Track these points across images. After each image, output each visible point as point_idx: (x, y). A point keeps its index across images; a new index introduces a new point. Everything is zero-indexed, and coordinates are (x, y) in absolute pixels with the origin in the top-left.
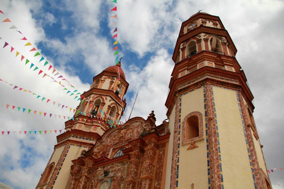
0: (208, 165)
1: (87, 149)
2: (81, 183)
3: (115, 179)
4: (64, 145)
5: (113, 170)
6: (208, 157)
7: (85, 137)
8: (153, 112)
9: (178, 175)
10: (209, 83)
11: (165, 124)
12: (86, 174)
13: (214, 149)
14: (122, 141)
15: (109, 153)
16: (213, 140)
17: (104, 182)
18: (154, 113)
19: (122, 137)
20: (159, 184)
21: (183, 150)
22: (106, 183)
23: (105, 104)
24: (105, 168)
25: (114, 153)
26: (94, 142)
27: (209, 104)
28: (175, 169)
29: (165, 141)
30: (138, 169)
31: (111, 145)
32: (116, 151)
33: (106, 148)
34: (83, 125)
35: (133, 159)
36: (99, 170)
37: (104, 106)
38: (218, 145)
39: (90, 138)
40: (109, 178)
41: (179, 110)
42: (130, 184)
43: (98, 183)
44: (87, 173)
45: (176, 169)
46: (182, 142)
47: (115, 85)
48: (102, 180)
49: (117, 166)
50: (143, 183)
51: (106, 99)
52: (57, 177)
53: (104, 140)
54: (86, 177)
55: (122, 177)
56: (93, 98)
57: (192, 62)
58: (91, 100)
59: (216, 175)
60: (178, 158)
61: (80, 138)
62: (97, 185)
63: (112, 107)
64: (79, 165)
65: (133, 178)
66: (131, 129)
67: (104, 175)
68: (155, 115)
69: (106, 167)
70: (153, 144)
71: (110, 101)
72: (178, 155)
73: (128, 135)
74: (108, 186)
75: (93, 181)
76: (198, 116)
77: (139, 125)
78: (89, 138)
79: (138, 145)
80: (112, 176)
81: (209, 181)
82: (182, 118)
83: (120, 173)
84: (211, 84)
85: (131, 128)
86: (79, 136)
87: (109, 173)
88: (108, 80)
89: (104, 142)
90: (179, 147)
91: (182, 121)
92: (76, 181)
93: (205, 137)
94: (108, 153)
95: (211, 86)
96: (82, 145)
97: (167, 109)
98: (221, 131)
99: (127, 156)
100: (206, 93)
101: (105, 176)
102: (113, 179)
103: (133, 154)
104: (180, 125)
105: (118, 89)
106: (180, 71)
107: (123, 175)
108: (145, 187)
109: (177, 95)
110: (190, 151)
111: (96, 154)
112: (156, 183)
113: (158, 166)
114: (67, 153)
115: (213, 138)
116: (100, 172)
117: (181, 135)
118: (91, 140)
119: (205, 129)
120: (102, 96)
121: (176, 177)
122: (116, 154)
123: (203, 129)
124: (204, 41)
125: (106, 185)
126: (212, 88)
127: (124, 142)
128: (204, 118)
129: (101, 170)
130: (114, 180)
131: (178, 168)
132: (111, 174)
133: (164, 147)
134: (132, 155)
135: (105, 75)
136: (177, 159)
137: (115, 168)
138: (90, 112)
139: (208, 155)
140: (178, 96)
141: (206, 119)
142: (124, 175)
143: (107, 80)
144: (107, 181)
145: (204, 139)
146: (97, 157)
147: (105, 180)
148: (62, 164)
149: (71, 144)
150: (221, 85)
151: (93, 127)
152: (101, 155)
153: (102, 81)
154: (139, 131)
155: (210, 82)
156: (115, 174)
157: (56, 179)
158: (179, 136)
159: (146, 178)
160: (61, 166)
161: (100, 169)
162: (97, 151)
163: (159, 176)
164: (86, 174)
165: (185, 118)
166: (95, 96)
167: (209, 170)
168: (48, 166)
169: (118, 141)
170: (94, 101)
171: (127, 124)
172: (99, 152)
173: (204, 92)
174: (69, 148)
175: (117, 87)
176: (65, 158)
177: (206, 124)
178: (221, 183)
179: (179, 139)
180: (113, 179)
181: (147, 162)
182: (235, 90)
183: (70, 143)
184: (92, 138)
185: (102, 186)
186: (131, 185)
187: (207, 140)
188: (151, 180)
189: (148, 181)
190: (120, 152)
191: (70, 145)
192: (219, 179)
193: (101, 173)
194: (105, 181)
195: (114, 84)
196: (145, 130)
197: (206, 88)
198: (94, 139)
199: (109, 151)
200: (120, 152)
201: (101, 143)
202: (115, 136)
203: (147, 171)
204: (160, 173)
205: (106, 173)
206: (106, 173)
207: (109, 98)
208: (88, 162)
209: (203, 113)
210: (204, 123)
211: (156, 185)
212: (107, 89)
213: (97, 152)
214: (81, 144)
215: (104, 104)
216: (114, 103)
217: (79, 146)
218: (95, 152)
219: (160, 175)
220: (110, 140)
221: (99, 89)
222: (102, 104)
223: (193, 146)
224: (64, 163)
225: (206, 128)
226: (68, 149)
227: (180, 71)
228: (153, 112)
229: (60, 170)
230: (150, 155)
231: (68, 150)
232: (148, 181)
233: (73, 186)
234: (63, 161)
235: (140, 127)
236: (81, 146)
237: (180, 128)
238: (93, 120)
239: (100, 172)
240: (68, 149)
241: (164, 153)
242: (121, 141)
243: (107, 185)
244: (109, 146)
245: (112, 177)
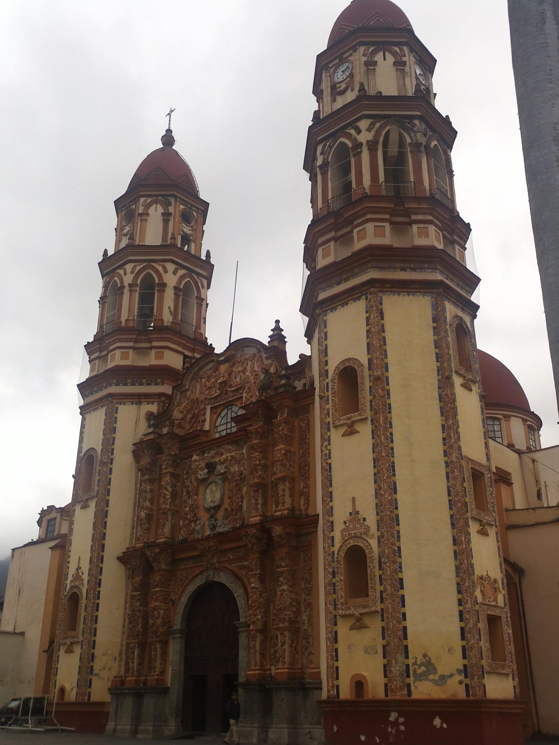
0: (375, 467)
1: (154, 408)
2: (166, 489)
3: (229, 477)
4: (102, 407)
5: (222, 460)
6: (373, 452)
7: (144, 381)
8: (277, 322)
9: (331, 480)
10: (376, 290)
11: (304, 360)
12: (171, 470)
13: (383, 437)
14: (226, 390)
15: (205, 418)
16: (381, 421)
17: (210, 484)
18: (281, 326)
19: (225, 382)
20: (307, 486)
21: (335, 435)
22: (213, 485)
23: (165, 285)
24: (206, 455)
25: (216, 416)
26: (166, 389)
27: (375, 343)
28: (327, 471)
29: (308, 402)
30: (267, 458)
31: (206, 399)
32: (219, 411)
33: (196, 405)
34: (131, 351)
35: (255, 442)
36: (195, 461)
37: (164, 291)
38: (389, 429)
39: (156, 381)
40: (218, 475)
41: (324, 348)
42: (258, 489)
43: (198, 484)
44: (172, 467)
45: (328, 470)
46: (334, 421)
47: (176, 220)
48: (204, 480)
49: (229, 451)
50: (280, 487)
51: (166, 271)
52: (110, 479)
53: (187, 387)
54: (172, 475)
55: (241, 474)
56: (132, 272)
57: (342, 220)
58: (131, 282)
59: (385, 485)
60: (330, 450)
61: (133, 384)
62: (197, 490)
63: (182, 287)
64: (150, 451)
65: (262, 478)
66: (239, 362)
67: (206, 470)
68: (283, 330)
69: (207, 451)
70: (286, 410)
71: (174, 273)
72: (329, 444)
73: (236, 378)
74: (219, 491)
75: (187, 483)
76: (356, 368)
77: (254, 355)
78: (152, 381)
79: (260, 412)
80: (222, 471)
81: (376, 494)
82: (332, 368)
83: (236, 465)
84: (379, 291)
85: (239, 360)
86: (129, 381)
87: (216, 465)
88: (156, 210)
89: (188, 390)
90: (329, 430)
91: (330, 374)
92: (153, 483)
93: (368, 413)
94: (203, 418)
95: (380, 294)
96: (142, 400)
97: (307, 319)
98: (396, 400)
99: (243, 433)
100: (370, 316)
101: (209, 472)
102: (225, 477)
103: (253, 431)
104: (327, 384)
105: (185, 230)
106: (320, 241)
107: (242, 469)
108: (284, 495)
109: (317, 311)
110: (346, 438)
111: (180, 423)
112: (302, 485)
113: (301, 451)
114: (115, 425)
115: (381, 415)
116: (197, 463)
117: (330, 406)
118: (157, 384)
119: (368, 398)
120: (154, 264)
121: (328, 484)
122: (220, 419)
123: (365, 396)
124: (369, 149)
125: (214, 488)
126: (381, 299)
127: (229, 393)
128: (366, 373)
129: (199, 461)
130: (228, 479)
131: (330, 468)
132: (221, 469)
133: (307, 413)
134: (251, 433)
135: (144, 196)
136: (328, 451)
137: (224, 456)
138: (136, 314)
139: (373, 448)
140: (319, 315)
141: (370, 376)
142: (244, 469)
143: (151, 211)
144: (216, 482)
145: (366, 418)
146: (184, 428)
147: (211, 479)
148: (113, 449)
149: (117, 403)
150: (400, 288)
151: (154, 351)
152: (190, 422)
153: (140, 215)
154: (256, 371)
155: (377, 287)
156: (226, 468)
157: (109, 484)
158: (328, 406)
159: (283, 479)
160: (112, 454)
161: (195, 457)
162: (180, 417)
163: (305, 470)
164: (171, 470)
165: (335, 370)
166: (138, 268)
167: (375, 475)
168: (82, 455)
169: (218, 392)
170: (139, 282)
171: (228, 353)
172: (184, 418)
173: (367, 312)
174: (117, 413)
175: (183, 225)
176: (114, 435)
177: (370, 387)
178: (394, 495)
179: (328, 413)
180: (225, 477)
181: (281, 449)
182: (429, 293)
183: (115, 401)
184: (159, 381)
185: (208, 491)
186: (260, 491)
187: (372, 420)
188: (292, 480)
189: (287, 483)
190: (227, 414)
191: (117, 406)
192: (390, 490)
193: (200, 466)
194: (212, 483)
195: (172, 219)
196: (266, 371)
197: (370, 302)
198: (163, 381)
199: (205, 413)
200: (227, 414)
201: (182, 393)
202: (209, 377)
203: (283, 465)
204: (306, 466)
205: (211, 467)
206: (211, 467)
207: (171, 267)
208: (169, 445)
209: (365, 362)
210: (367, 384)
211: (302, 487)
212: (159, 243)
213: (180, 419)
214: (139, 399)
215: (163, 286)
216: (186, 274)
217: (136, 404)
218: (177, 420)
219: (307, 468)
220: (201, 386)
221: (139, 246)
222: (158, 286)
223: (351, 432)
224: (116, 447)
225: (370, 395)
226: (116, 415)
227: (320, 241)
228: (277, 322)
229: (111, 464)
230: (285, 434)
231: (116, 418)
232: (287, 483)
233: (150, 494)
234: (113, 444)
235: (256, 358)
236: (140, 403)
237: (328, 391)
238: (151, 336)
239: (197, 463)
240: (116, 415)
241: (308, 425)
242: (224, 392)
243: (217, 489)
244: (202, 402)
245: (222, 474)
